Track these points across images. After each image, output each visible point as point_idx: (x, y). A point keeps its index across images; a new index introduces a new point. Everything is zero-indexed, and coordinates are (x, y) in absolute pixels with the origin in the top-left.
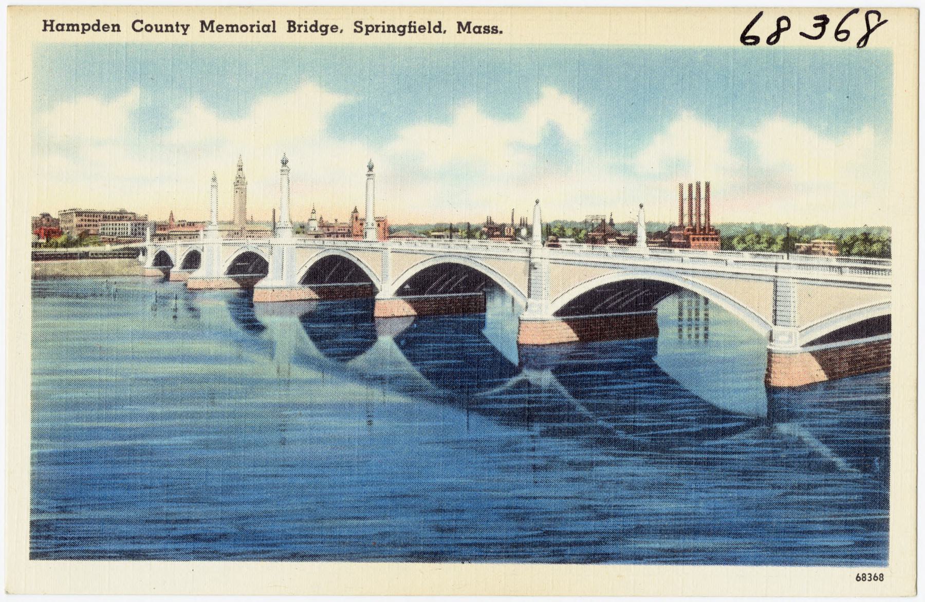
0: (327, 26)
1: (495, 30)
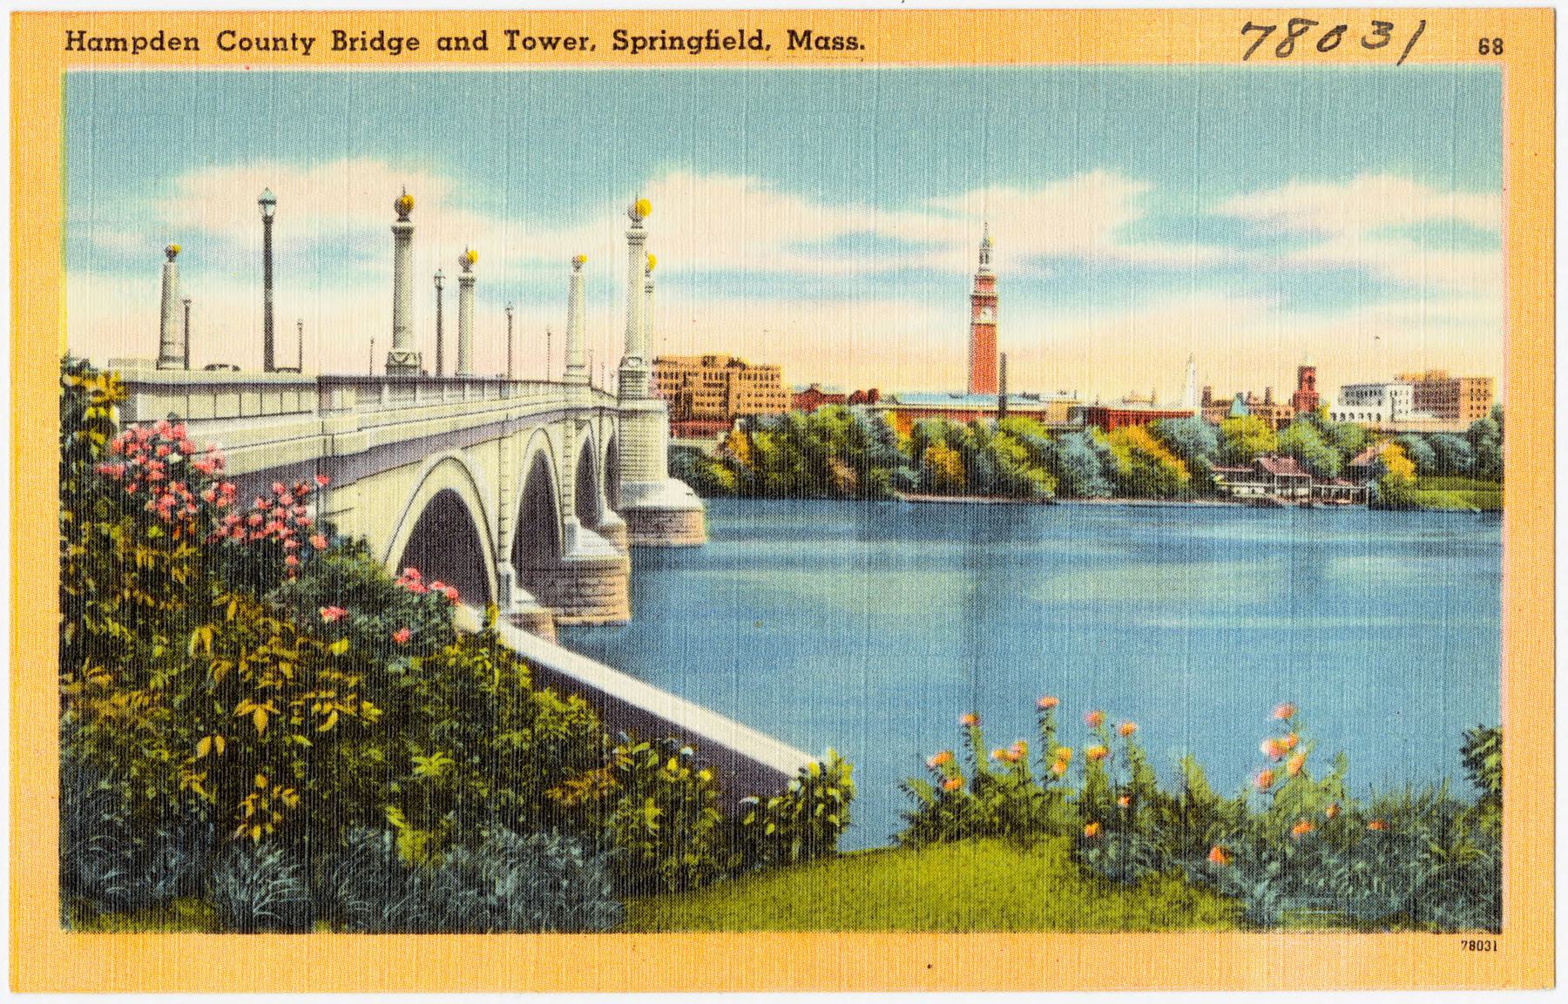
0: (399, 40)
1: (853, 44)
